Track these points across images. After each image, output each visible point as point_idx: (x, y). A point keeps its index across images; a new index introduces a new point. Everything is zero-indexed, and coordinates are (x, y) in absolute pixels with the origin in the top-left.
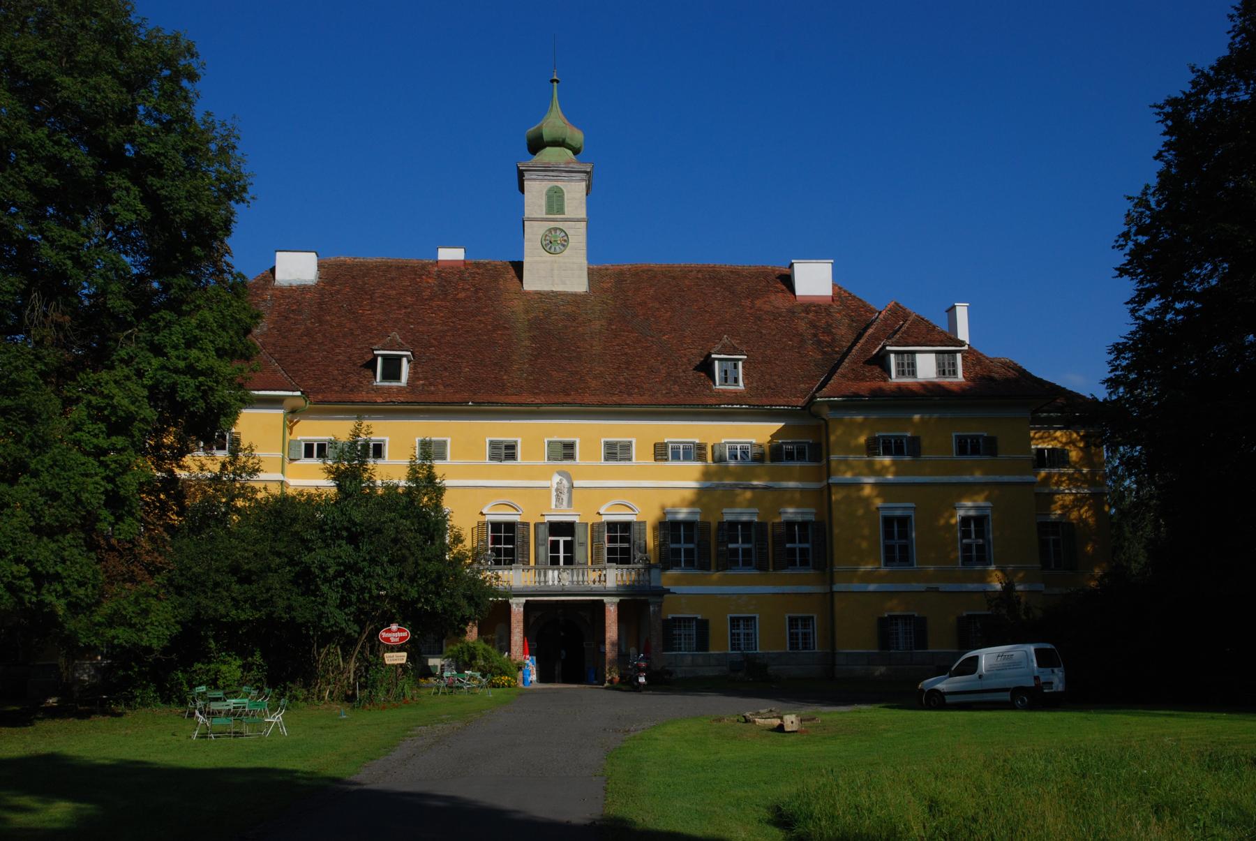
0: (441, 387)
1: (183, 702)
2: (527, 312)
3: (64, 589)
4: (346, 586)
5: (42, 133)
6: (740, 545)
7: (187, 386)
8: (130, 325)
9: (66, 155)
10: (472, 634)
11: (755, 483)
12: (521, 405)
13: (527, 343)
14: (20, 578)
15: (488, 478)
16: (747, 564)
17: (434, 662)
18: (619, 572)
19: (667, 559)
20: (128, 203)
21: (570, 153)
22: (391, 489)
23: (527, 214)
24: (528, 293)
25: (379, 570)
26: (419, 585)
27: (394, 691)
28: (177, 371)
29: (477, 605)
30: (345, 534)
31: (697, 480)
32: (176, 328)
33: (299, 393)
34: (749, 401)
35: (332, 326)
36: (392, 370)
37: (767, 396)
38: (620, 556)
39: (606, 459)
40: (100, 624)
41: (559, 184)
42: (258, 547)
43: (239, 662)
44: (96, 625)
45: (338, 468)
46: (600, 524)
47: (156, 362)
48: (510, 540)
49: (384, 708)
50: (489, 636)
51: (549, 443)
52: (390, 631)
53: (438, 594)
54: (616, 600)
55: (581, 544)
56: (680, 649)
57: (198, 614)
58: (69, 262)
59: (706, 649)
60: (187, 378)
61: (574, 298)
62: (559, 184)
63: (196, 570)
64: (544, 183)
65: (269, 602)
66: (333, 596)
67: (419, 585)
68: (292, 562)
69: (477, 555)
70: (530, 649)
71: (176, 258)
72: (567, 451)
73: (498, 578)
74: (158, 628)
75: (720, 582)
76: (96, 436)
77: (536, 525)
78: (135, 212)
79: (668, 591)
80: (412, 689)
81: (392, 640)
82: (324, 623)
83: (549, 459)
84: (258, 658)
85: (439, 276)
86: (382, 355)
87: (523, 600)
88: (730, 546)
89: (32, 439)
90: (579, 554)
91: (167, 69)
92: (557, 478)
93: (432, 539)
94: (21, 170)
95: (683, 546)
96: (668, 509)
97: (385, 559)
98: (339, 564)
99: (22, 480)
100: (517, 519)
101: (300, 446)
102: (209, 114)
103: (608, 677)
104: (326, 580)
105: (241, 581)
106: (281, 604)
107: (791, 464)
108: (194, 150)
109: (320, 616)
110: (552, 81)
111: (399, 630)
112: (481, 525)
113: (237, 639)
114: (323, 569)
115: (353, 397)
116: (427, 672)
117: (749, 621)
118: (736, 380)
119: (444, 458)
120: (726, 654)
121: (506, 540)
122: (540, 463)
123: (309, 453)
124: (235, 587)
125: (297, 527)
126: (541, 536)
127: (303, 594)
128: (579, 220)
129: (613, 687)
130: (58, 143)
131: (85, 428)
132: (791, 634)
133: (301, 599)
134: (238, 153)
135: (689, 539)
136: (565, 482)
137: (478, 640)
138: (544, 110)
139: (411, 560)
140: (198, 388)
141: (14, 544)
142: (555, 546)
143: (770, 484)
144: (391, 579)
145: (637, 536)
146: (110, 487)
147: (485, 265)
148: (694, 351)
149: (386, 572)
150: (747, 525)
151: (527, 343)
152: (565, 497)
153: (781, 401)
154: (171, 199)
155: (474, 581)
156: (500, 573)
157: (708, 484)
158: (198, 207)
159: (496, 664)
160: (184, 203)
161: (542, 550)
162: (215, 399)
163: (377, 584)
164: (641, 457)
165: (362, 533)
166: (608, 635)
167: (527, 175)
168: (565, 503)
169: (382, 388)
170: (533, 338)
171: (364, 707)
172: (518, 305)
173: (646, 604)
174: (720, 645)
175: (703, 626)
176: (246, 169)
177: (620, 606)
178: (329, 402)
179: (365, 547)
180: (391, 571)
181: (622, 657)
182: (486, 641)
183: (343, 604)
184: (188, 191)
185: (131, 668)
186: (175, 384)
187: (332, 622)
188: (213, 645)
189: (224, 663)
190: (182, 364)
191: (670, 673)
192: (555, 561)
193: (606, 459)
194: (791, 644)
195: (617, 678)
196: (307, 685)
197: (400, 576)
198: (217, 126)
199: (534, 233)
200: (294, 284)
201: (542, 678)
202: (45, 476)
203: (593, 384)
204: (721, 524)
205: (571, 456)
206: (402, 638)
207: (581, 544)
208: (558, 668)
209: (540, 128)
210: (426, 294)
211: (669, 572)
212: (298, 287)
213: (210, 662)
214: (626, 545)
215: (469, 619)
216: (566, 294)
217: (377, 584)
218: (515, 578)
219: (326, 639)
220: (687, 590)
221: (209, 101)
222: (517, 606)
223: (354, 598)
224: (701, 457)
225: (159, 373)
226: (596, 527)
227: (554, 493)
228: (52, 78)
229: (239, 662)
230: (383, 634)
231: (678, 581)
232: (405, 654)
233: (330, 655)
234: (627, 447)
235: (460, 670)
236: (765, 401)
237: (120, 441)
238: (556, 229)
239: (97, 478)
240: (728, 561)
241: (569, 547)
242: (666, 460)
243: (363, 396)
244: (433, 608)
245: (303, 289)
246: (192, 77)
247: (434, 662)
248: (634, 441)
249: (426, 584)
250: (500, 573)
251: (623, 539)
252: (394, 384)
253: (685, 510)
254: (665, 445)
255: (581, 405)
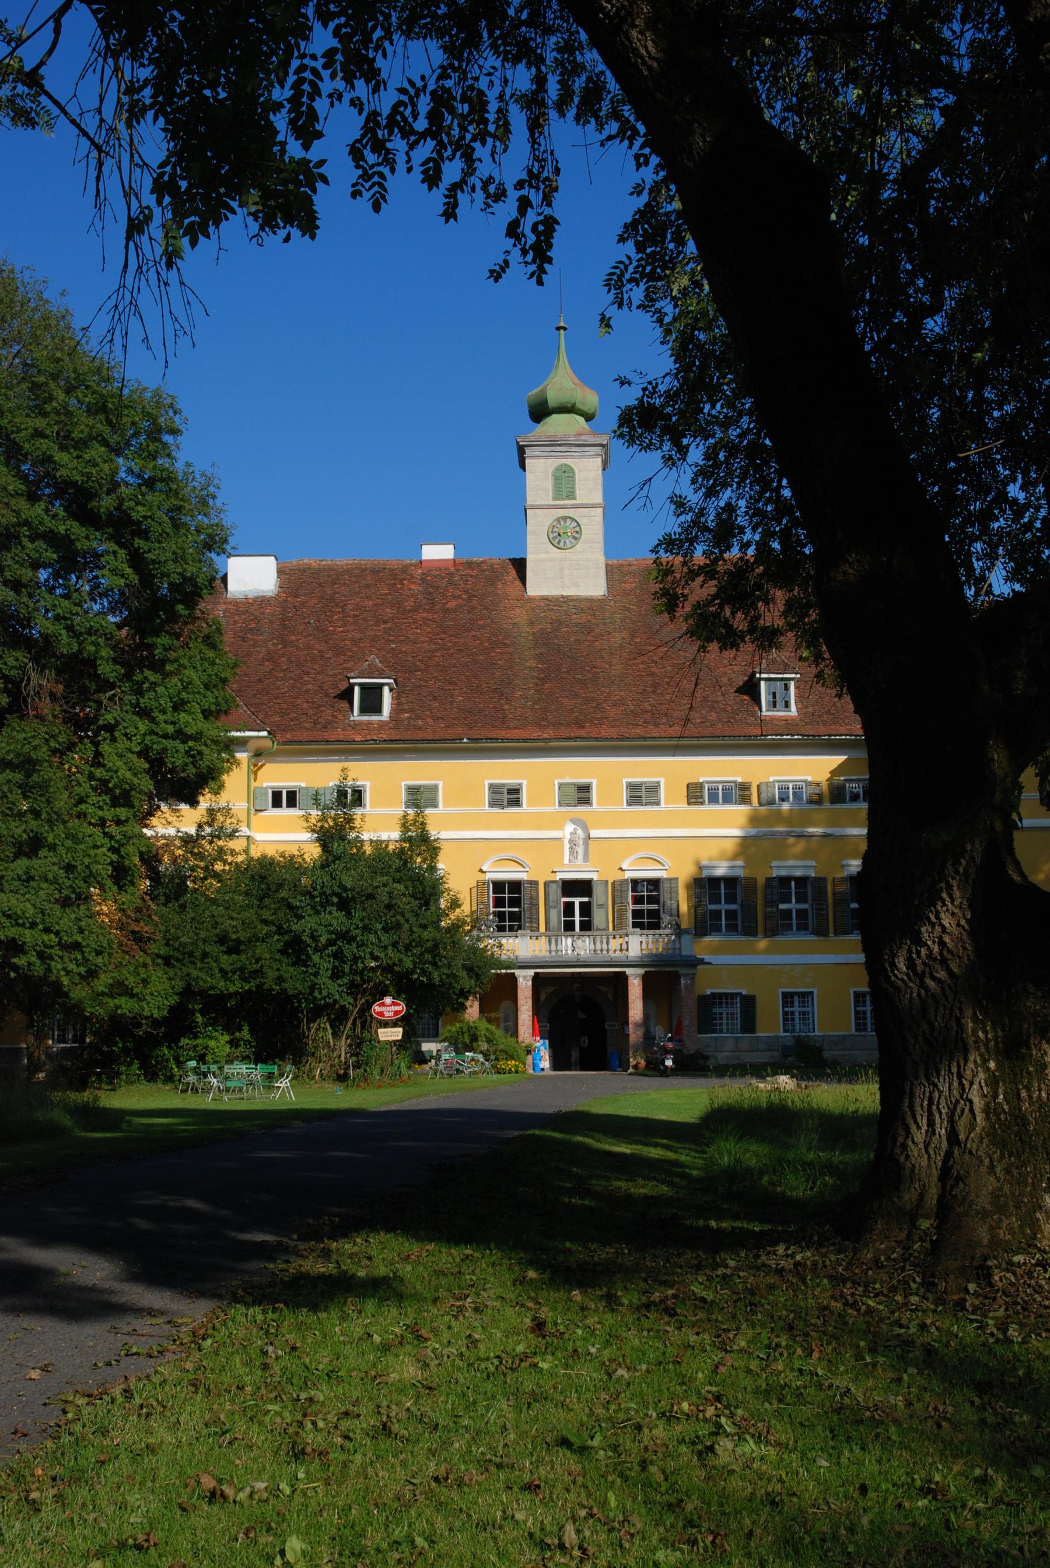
0: (430, 721)
1: (169, 1079)
2: (532, 624)
3: (84, 958)
4: (338, 955)
5: (39, 509)
6: (793, 906)
7: (177, 751)
8: (112, 686)
9: (62, 529)
10: (473, 1010)
11: (811, 830)
12: (525, 740)
13: (532, 663)
14: (51, 947)
15: (488, 828)
16: (802, 927)
17: (429, 1047)
18: (644, 939)
19: (704, 924)
20: (115, 572)
21: (581, 420)
22: (378, 845)
23: (530, 501)
24: (532, 599)
25: (372, 938)
26: (413, 955)
27: (389, 1071)
28: (166, 736)
29: (478, 977)
30: (335, 900)
31: (742, 828)
32: (160, 690)
33: (265, 734)
34: (803, 731)
35: (298, 648)
36: (372, 701)
37: (825, 723)
38: (647, 919)
39: (629, 804)
40: (103, 994)
41: (569, 462)
42: (244, 915)
43: (227, 1038)
44: (98, 994)
45: (322, 827)
46: (624, 882)
47: (143, 726)
48: (516, 902)
49: (380, 1087)
50: (493, 1015)
51: (561, 785)
52: (383, 1005)
53: (434, 964)
54: (641, 971)
55: (601, 906)
56: (721, 1031)
57: (189, 985)
58: (63, 632)
59: (753, 1031)
60: (177, 744)
61: (590, 605)
62: (569, 462)
63: (183, 939)
64: (549, 461)
65: (258, 973)
66: (324, 964)
67: (413, 955)
68: (280, 931)
69: (476, 922)
70: (540, 1031)
71: (159, 617)
72: (582, 794)
73: (500, 946)
74: (157, 997)
75: (767, 951)
76: (101, 808)
77: (547, 884)
78: (123, 576)
79: (702, 962)
80: (409, 1068)
81: (386, 1014)
82: (316, 994)
83: (560, 805)
84: (245, 1033)
85: (423, 580)
86: (359, 684)
87: (531, 972)
88: (782, 906)
89: (48, 814)
90: (598, 917)
91: (149, 428)
92: (570, 828)
93: (427, 904)
94: (23, 548)
95: (723, 907)
96: (704, 863)
97: (379, 926)
98: (330, 932)
99: (41, 854)
100: (523, 876)
101: (266, 794)
102: (188, 465)
103: (632, 1062)
104: (316, 950)
105: (229, 952)
106: (271, 974)
107: (854, 806)
108: (180, 509)
109: (312, 988)
110: (558, 329)
111: (394, 1004)
112: (481, 885)
113: (223, 1012)
114: (314, 938)
115: (326, 735)
116: (421, 1058)
117: (805, 996)
118: (787, 705)
119: (436, 806)
120: (778, 1037)
121: (510, 902)
122: (550, 809)
123: (277, 802)
124: (224, 958)
125: (284, 894)
126: (552, 897)
127: (293, 964)
128: (593, 506)
129: (638, 1072)
130: (54, 517)
131: (90, 801)
132: (857, 1013)
133: (291, 969)
134: (218, 502)
135: (731, 899)
136: (580, 832)
137: (480, 1019)
138: (549, 366)
139: (406, 926)
140: (187, 752)
141: (44, 915)
142: (569, 909)
143: (829, 831)
144: (386, 947)
145: (667, 896)
146: (115, 857)
147: (479, 564)
148: (736, 668)
149: (380, 941)
150: (802, 881)
151: (532, 663)
152: (580, 850)
153: (842, 730)
154: (159, 562)
155: (474, 950)
156: (504, 941)
157: (753, 832)
158: (185, 570)
159: (501, 1047)
160: (171, 566)
161: (553, 914)
162: (204, 763)
163: (371, 953)
164: (672, 800)
165: (354, 898)
166: (631, 1013)
167: (527, 450)
168: (580, 857)
169: (361, 723)
170: (539, 657)
171: (358, 1086)
172: (520, 615)
173: (677, 977)
174: (771, 1026)
175: (749, 1003)
176: (227, 520)
177: (646, 979)
178: (300, 742)
179: (358, 914)
180: (385, 938)
181: (648, 1038)
182: (489, 1021)
183: (336, 974)
184: (174, 553)
185: (115, 1044)
186: (165, 749)
187: (325, 993)
188: (199, 1019)
189: (211, 1038)
190: (170, 729)
191: (707, 1058)
192: (569, 926)
193: (629, 804)
194: (857, 1025)
195: (643, 1063)
196: (296, 1063)
197: (395, 945)
198: (197, 476)
199: (538, 524)
200: (251, 596)
201: (556, 1065)
202: (61, 850)
203: (612, 713)
204: (769, 880)
205: (586, 801)
206: (396, 1013)
207: (601, 906)
208: (575, 1054)
209: (543, 391)
210: (409, 604)
211: (707, 939)
212: (255, 599)
213: (196, 1037)
214: (654, 907)
215: (469, 992)
216: (579, 599)
217: (371, 953)
218: (522, 947)
219: (316, 1013)
220: (729, 961)
221: (191, 453)
222: (525, 980)
223: (347, 968)
224: (745, 800)
225: (148, 738)
226: (618, 887)
227: (567, 846)
228: (51, 456)
229: (227, 1038)
230: (376, 1008)
231: (718, 950)
232: (401, 1030)
233: (320, 1032)
234: (653, 789)
235: (457, 1051)
236: (822, 730)
237: (123, 812)
238: (565, 518)
239: (105, 850)
240: (779, 925)
241: (586, 909)
242: (702, 803)
243: (339, 734)
244: (430, 979)
245: (261, 602)
246: (174, 432)
247: (429, 1047)
248: (662, 781)
249: (422, 954)
250: (504, 941)
251: (652, 900)
252: (375, 718)
253: (725, 864)
254: (700, 786)
255: (597, 739)
